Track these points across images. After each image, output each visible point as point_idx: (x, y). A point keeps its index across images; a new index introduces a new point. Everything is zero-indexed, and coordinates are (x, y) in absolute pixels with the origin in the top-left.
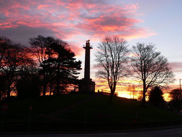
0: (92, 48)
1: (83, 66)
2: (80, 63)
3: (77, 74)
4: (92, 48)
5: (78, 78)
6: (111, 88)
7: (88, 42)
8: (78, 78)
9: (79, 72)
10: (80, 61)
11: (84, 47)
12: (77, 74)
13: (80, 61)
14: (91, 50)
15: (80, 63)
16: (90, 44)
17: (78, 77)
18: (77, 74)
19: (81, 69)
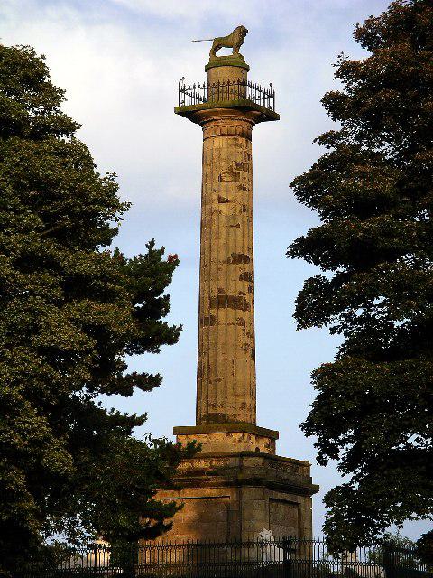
0: (306, 436)
1: (183, 301)
2: (156, 269)
3: (128, 393)
4: (271, 116)
5: (138, 433)
6: (262, 437)
7: (224, 52)
8: (138, 433)
9: (152, 372)
10: (154, 255)
11: (188, 101)
12: (128, 393)
13: (154, 255)
14: (304, 420)
15: (156, 269)
16: (251, 77)
17: (140, 421)
18: (124, 388)
19: (171, 336)
